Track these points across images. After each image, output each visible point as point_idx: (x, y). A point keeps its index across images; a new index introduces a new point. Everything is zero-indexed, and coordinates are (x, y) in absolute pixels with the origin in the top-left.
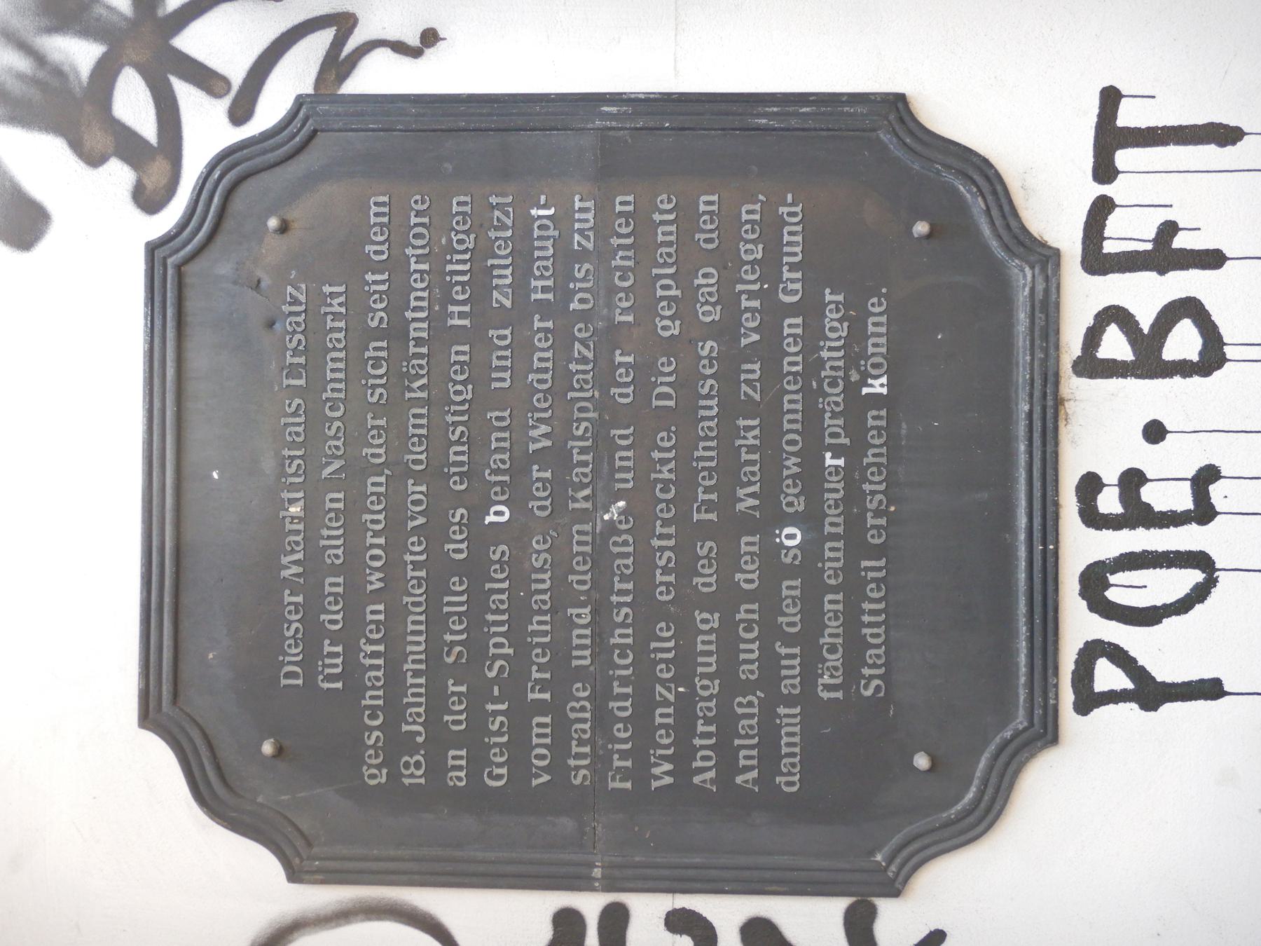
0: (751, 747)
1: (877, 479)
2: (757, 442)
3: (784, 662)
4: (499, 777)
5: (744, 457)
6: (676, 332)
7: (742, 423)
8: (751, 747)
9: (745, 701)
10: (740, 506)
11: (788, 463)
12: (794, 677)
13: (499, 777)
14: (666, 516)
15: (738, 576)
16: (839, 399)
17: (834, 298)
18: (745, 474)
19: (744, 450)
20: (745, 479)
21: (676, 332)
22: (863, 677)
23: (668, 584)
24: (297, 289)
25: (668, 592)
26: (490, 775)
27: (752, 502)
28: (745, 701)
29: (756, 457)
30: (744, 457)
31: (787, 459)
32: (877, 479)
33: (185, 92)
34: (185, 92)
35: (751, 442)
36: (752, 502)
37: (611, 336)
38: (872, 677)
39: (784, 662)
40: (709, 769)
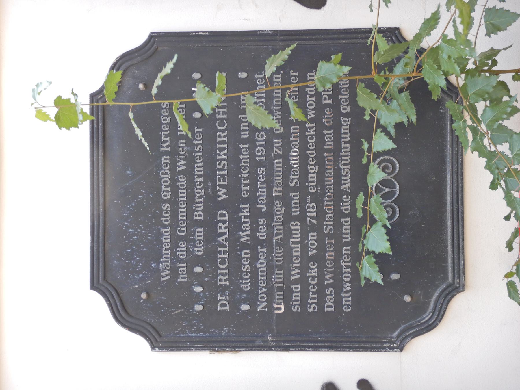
2: (248, 214)
4: (183, 231)
5: (243, 220)
7: (242, 206)
9: (294, 224)
10: (242, 240)
11: (310, 113)
12: (331, 185)
13: (183, 231)
15: (259, 234)
16: (297, 169)
18: (244, 227)
19: (243, 217)
20: (244, 229)
22: (309, 303)
23: (246, 191)
25: (247, 194)
26: (179, 231)
27: (247, 238)
28: (294, 224)
29: (248, 220)
30: (243, 220)
31: (309, 112)
35: (246, 214)
36: (247, 238)
38: (312, 303)
40: (261, 294)
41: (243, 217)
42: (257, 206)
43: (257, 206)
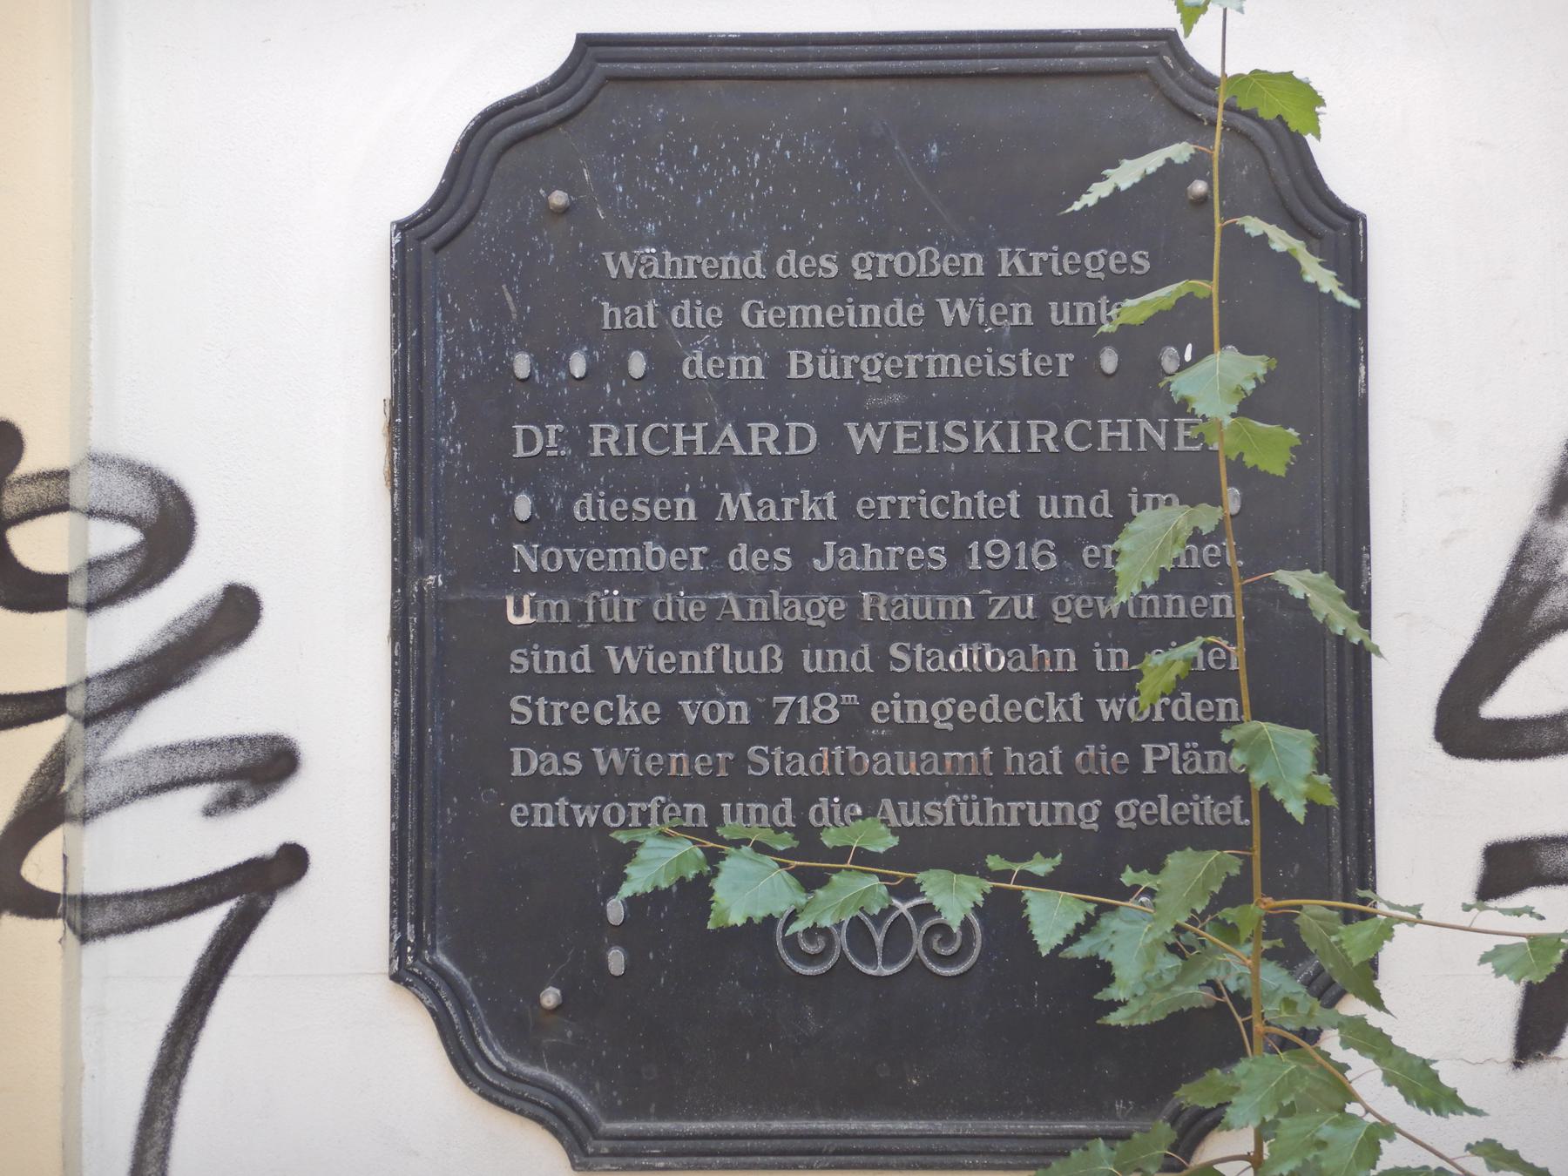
0: (974, 511)
1: (991, 508)
2: (806, 517)
3: (750, 655)
5: (788, 501)
6: (858, 276)
7: (830, 497)
8: (974, 511)
14: (910, 558)
17: (696, 557)
19: (797, 501)
20: (760, 503)
21: (1121, 824)
24: (1157, 426)
27: (732, 512)
29: (788, 516)
30: (788, 501)
32: (991, 508)
33: (208, 923)
34: (208, 923)
35: (806, 511)
36: (732, 512)
37: (762, 727)
38: (535, 709)
39: (750, 655)
41: (797, 501)
42: (830, 544)
43: (830, 544)
